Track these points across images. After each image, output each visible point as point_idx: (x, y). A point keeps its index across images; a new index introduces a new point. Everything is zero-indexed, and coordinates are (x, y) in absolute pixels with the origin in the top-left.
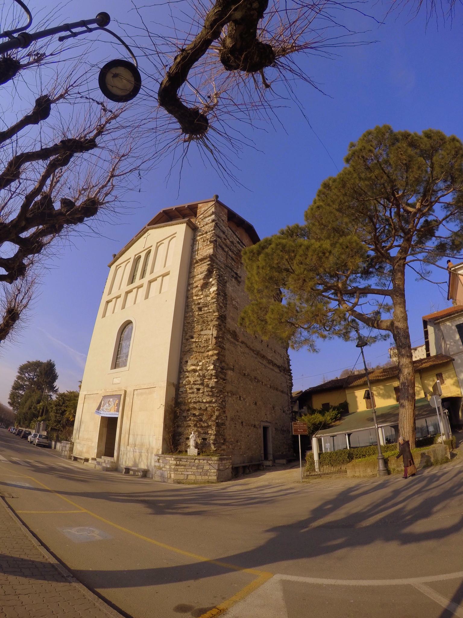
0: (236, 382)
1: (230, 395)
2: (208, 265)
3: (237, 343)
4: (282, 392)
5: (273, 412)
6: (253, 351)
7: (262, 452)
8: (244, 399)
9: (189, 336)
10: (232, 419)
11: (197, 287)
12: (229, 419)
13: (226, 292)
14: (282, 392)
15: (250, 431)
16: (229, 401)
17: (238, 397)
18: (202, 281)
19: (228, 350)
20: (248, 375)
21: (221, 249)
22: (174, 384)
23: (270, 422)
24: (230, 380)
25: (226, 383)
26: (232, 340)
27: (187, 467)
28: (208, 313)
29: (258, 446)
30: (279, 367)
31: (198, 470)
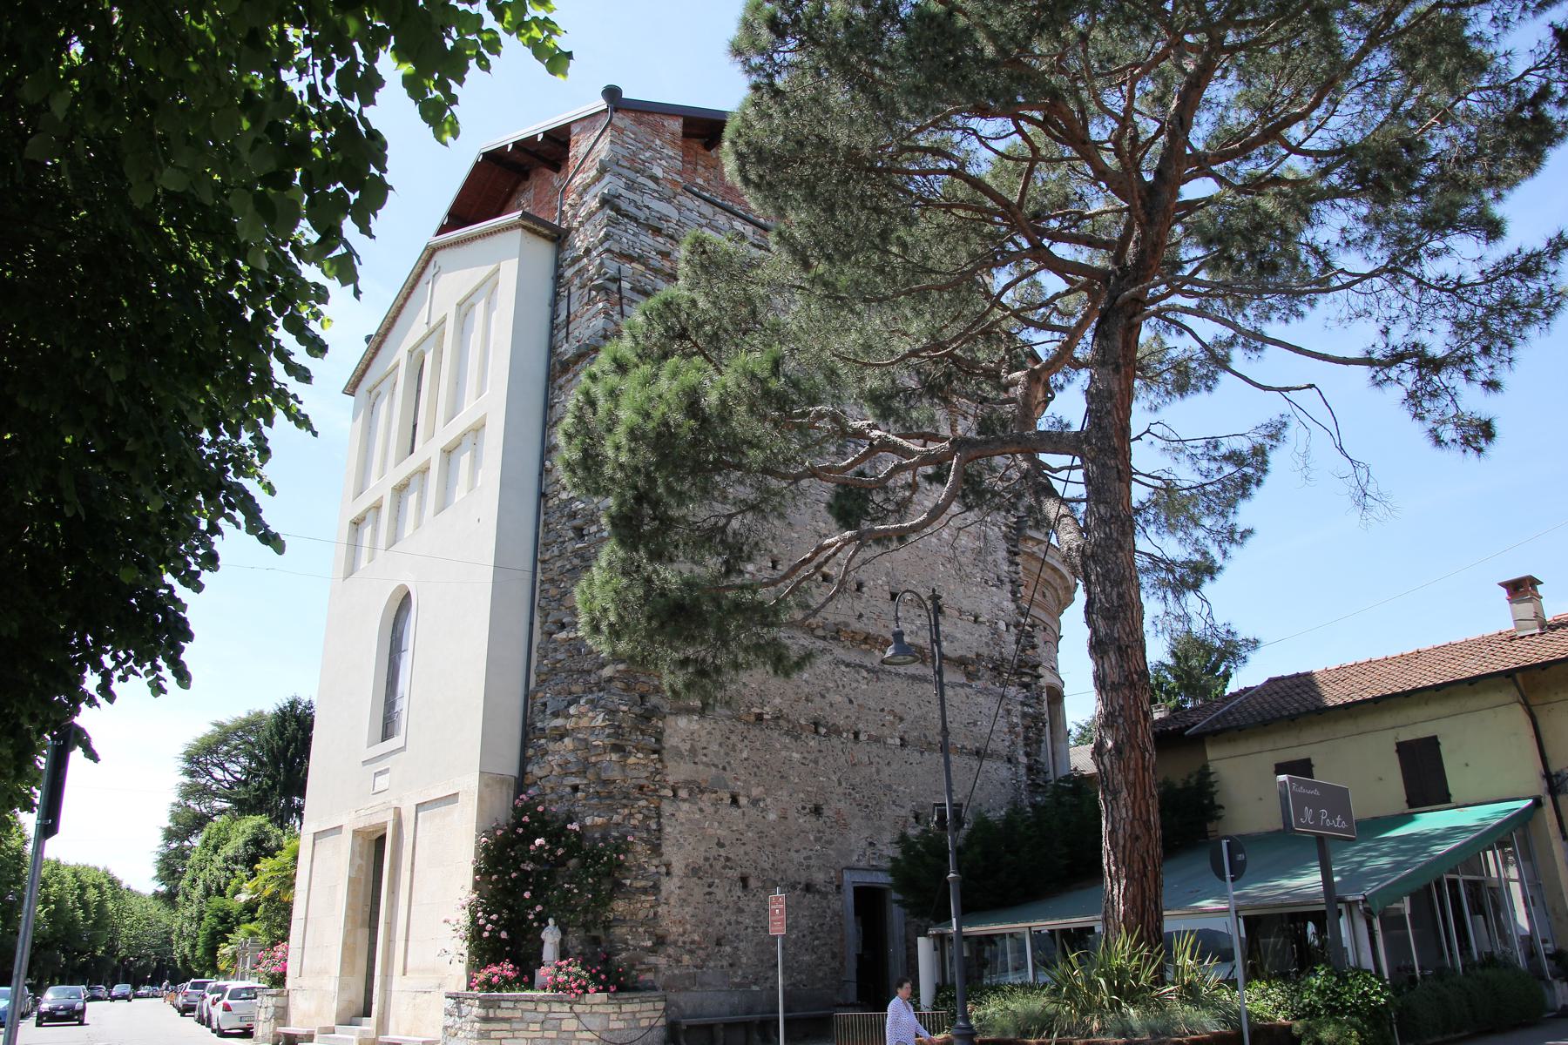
0: (716, 748)
9: (554, 623)
10: (695, 871)
12: (678, 867)
16: (681, 816)
22: (501, 780)
24: (685, 747)
27: (515, 1026)
31: (547, 1034)
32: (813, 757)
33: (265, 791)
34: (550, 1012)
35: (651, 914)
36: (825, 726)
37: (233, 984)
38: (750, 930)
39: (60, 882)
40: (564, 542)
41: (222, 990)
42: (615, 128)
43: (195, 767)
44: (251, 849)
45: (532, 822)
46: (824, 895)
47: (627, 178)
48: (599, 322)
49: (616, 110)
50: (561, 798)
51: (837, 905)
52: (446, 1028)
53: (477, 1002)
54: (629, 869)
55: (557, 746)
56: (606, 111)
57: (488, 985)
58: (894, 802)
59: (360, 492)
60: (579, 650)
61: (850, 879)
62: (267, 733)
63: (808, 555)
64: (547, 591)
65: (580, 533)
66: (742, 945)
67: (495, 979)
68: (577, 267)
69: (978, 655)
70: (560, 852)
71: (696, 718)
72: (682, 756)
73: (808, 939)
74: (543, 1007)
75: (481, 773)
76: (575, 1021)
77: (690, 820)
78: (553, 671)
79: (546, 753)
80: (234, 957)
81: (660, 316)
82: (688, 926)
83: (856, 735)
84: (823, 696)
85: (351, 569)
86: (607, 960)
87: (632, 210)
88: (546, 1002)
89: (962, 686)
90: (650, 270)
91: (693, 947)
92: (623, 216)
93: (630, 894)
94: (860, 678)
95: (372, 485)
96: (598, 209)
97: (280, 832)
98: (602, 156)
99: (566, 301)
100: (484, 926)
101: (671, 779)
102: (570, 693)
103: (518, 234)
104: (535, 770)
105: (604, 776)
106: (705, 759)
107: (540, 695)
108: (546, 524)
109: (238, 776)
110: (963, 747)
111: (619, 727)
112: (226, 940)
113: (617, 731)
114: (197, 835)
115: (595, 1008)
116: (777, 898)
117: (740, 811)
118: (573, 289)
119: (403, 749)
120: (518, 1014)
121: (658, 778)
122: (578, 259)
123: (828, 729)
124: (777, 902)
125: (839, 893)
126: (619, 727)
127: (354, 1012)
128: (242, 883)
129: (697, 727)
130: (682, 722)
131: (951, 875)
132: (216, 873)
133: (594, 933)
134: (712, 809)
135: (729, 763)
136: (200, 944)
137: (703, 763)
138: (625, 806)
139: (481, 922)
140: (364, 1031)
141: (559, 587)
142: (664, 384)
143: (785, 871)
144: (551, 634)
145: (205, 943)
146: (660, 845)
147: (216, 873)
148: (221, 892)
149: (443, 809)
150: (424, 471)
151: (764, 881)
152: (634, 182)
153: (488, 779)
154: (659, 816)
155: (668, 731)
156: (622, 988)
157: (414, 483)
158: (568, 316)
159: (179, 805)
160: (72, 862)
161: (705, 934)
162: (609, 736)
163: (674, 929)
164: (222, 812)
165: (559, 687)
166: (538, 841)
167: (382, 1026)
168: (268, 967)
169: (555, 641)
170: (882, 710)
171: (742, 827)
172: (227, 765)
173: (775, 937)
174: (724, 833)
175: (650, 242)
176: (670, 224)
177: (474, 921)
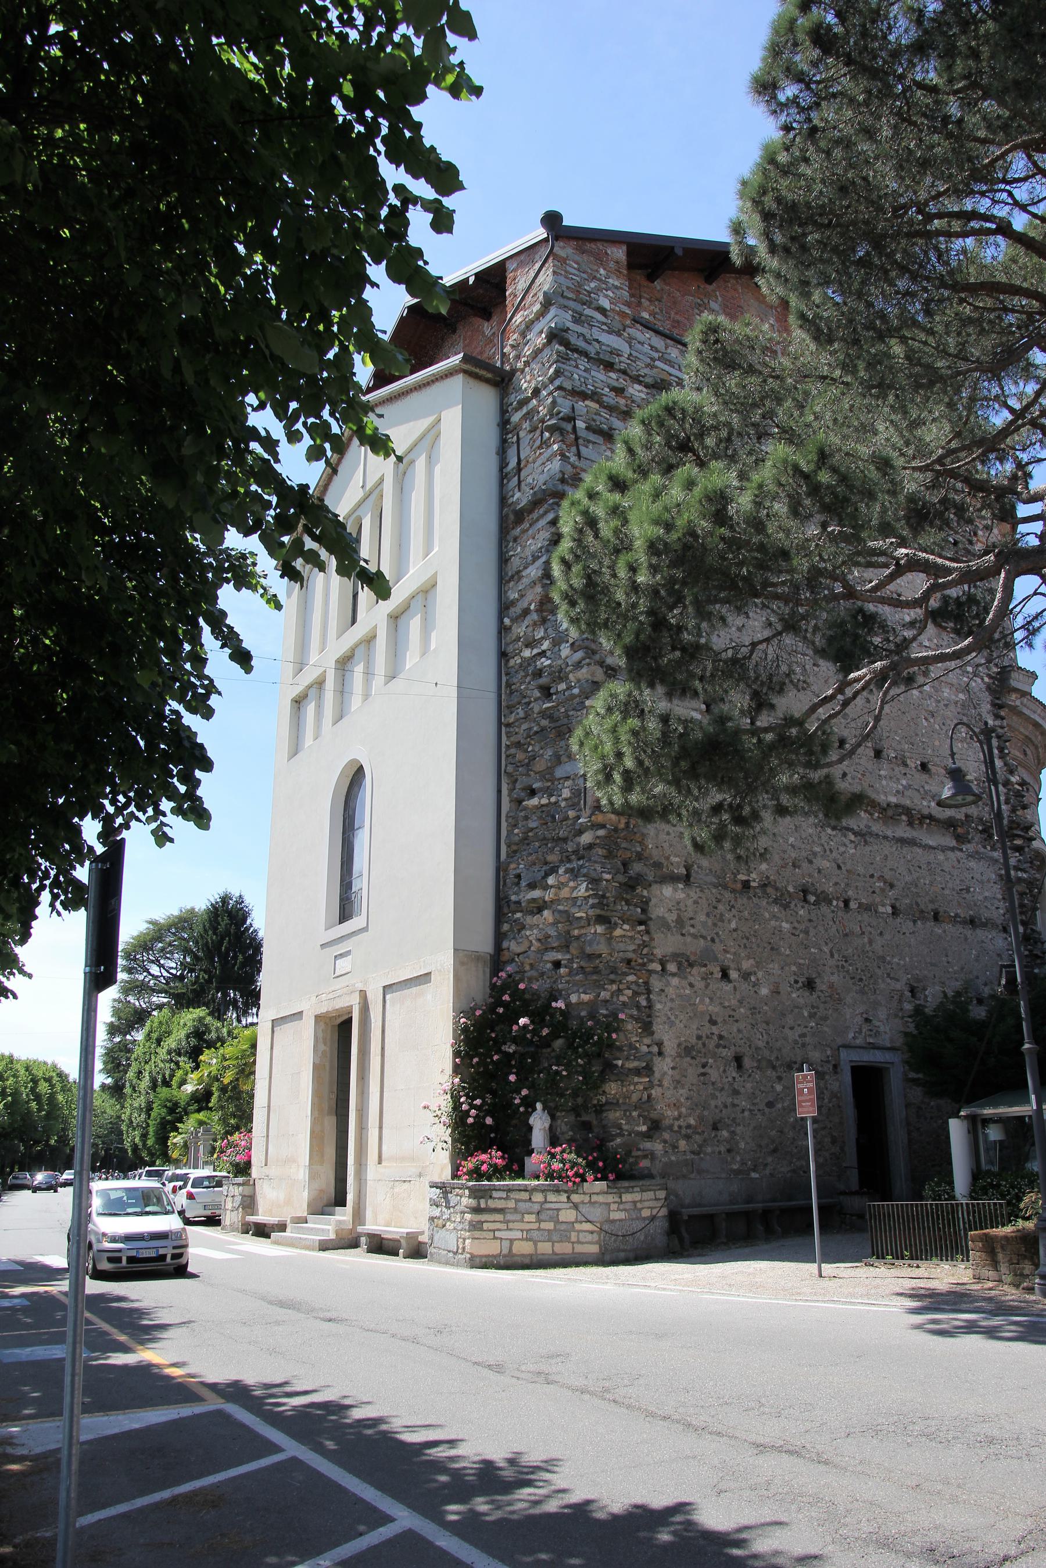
1: (672, 967)
9: (523, 789)
10: (687, 1051)
11: (526, 612)
12: (670, 1047)
16: (671, 991)
20: (764, 886)
21: (600, 440)
22: (477, 957)
24: (671, 918)
27: (509, 1217)
31: (543, 1225)
32: (803, 927)
34: (546, 1202)
35: (645, 1097)
36: (814, 894)
37: (195, 1173)
38: (746, 1113)
39: (14, 1076)
40: (529, 703)
41: (184, 1178)
42: (556, 258)
43: (133, 964)
44: (193, 1041)
45: (513, 1001)
47: (574, 311)
48: (556, 465)
49: (556, 238)
50: (542, 974)
52: (432, 1219)
53: (467, 1192)
54: (620, 1049)
55: (536, 919)
56: (546, 240)
57: (477, 1174)
58: (888, 975)
59: (300, 665)
60: (554, 817)
61: (847, 1058)
62: (201, 928)
63: (830, 692)
64: (514, 756)
65: (546, 692)
66: (739, 1130)
67: (484, 1167)
68: (525, 410)
71: (681, 886)
72: (669, 928)
74: (538, 1197)
75: (455, 950)
77: (680, 996)
78: (525, 840)
80: (186, 1145)
81: (661, 424)
82: (683, 1110)
83: (846, 903)
84: (810, 862)
85: (295, 749)
86: (601, 1146)
87: (581, 344)
88: (543, 1191)
89: (952, 849)
90: (605, 407)
91: (689, 1131)
92: (573, 350)
93: (623, 1075)
94: (847, 842)
96: (545, 346)
98: (546, 288)
100: (468, 1111)
101: (658, 952)
102: (546, 863)
103: (458, 381)
104: (513, 946)
105: (588, 950)
106: (692, 930)
107: (512, 866)
108: (509, 685)
109: (174, 971)
110: (957, 915)
111: (603, 896)
112: (176, 1129)
113: (602, 901)
114: (138, 1031)
115: (594, 1198)
116: (806, 1076)
117: (731, 985)
118: (522, 434)
119: (365, 929)
120: (511, 1204)
121: (645, 951)
122: (526, 401)
123: (817, 896)
124: (805, 1083)
125: (836, 1073)
126: (603, 896)
127: (325, 1202)
128: (186, 1074)
129: (683, 896)
130: (667, 891)
131: (1027, 1046)
132: (161, 1065)
133: (585, 1118)
134: (702, 984)
135: (717, 934)
136: (151, 1133)
137: (690, 934)
138: (613, 982)
139: (465, 1107)
140: (340, 1222)
141: (526, 751)
142: (676, 493)
143: (780, 1050)
144: (520, 802)
145: (156, 1133)
146: (651, 1023)
147: (161, 1065)
148: (167, 1084)
149: (414, 990)
150: (370, 640)
151: (759, 1061)
152: (581, 315)
153: (463, 957)
154: (649, 992)
155: (653, 901)
156: (620, 1176)
157: (359, 653)
159: (119, 1001)
160: (24, 1058)
161: (701, 1119)
162: (593, 906)
163: (669, 1113)
164: (160, 1007)
165: (534, 857)
166: (522, 1021)
167: (359, 1216)
168: (233, 1156)
169: (525, 808)
170: (872, 876)
171: (734, 1002)
172: (162, 962)
174: (716, 1010)
175: (604, 378)
176: (622, 359)
177: (456, 1106)
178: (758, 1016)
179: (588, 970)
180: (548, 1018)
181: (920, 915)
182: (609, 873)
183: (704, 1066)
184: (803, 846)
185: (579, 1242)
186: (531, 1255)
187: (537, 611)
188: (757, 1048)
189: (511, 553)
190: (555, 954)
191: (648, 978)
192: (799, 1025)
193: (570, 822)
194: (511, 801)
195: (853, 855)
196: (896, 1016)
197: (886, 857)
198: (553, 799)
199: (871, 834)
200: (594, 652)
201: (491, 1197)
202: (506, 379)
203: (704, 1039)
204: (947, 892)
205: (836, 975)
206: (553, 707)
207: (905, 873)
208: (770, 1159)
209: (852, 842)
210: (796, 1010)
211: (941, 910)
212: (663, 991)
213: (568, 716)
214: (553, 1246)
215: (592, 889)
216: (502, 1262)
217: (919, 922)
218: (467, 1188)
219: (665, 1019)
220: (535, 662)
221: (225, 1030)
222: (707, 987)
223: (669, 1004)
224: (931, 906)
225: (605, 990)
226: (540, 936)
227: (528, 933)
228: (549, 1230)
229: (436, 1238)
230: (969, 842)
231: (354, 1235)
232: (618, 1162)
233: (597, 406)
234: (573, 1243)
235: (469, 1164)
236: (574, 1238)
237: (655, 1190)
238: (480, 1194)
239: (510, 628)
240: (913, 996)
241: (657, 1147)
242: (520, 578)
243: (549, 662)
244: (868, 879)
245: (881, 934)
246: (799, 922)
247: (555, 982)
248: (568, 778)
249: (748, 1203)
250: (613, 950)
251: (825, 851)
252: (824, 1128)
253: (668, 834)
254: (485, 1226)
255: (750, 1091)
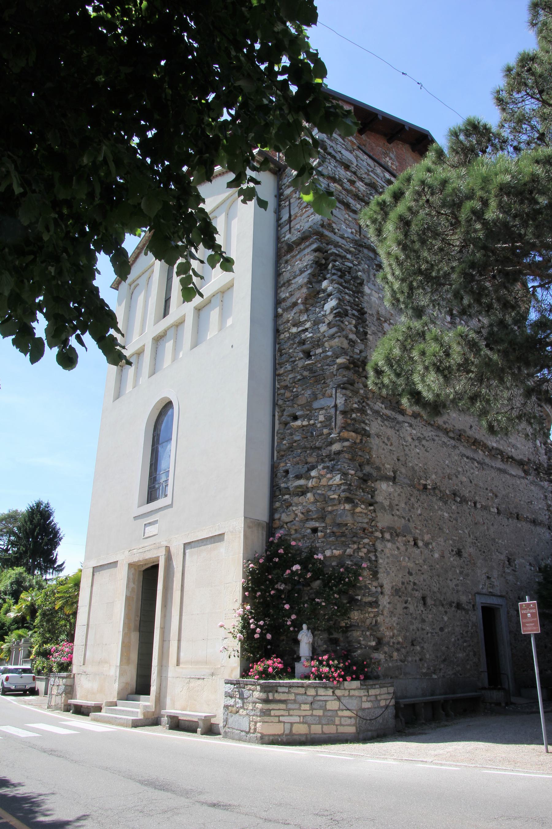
1: (387, 536)
2: (315, 250)
3: (400, 418)
4: (534, 522)
5: (507, 571)
6: (446, 432)
7: (483, 667)
8: (427, 544)
9: (289, 416)
10: (397, 592)
11: (295, 304)
13: (365, 305)
14: (534, 522)
15: (446, 618)
16: (387, 551)
17: (411, 539)
18: (304, 290)
19: (378, 436)
20: (434, 489)
21: (342, 207)
22: (258, 524)
23: (501, 596)
24: (386, 503)
25: (375, 511)
26: (388, 412)
27: (290, 706)
28: (323, 358)
29: (471, 653)
30: (521, 463)
31: (316, 712)
33: (21, 554)
34: (317, 695)
36: (459, 497)
38: (429, 635)
40: (294, 361)
46: (467, 611)
50: (304, 537)
51: (474, 619)
52: (226, 707)
53: (258, 688)
57: (264, 674)
58: (497, 550)
60: (312, 433)
61: (481, 601)
65: (308, 355)
69: (529, 460)
70: (309, 575)
73: (460, 642)
74: (311, 692)
75: (245, 518)
76: (337, 703)
77: (392, 555)
78: (291, 448)
79: (291, 505)
80: (9, 651)
83: (475, 503)
84: (457, 477)
85: (118, 394)
88: (315, 687)
89: (523, 478)
91: (399, 646)
94: (474, 467)
95: (134, 341)
97: (31, 577)
99: (287, 208)
100: (255, 629)
101: (380, 525)
102: (307, 463)
105: (339, 520)
106: (398, 513)
107: (282, 464)
110: (527, 517)
111: (350, 485)
115: (352, 693)
118: (292, 201)
119: (171, 506)
120: (292, 697)
121: (373, 524)
123: (461, 498)
126: (350, 485)
127: (129, 691)
129: (392, 490)
133: (335, 635)
135: (411, 516)
137: (397, 515)
138: (354, 543)
139: (252, 626)
140: (146, 706)
143: (445, 594)
144: (286, 424)
150: (179, 324)
151: (435, 600)
154: (376, 550)
156: (367, 678)
157: (170, 333)
158: (290, 216)
162: (344, 491)
163: (387, 633)
167: (160, 701)
169: (291, 428)
171: (421, 561)
173: (529, 636)
177: (246, 625)
178: (434, 571)
179: (337, 534)
180: (311, 566)
181: (510, 515)
182: (353, 470)
183: (406, 602)
184: (453, 467)
185: (341, 725)
186: (306, 734)
187: (303, 303)
188: (434, 592)
189: (284, 270)
190: (314, 523)
191: (375, 542)
192: (455, 578)
193: (324, 437)
194: (280, 423)
195: (477, 475)
196: (502, 576)
197: (493, 479)
198: (312, 422)
199: (485, 463)
200: (343, 330)
201: (277, 691)
202: (282, 170)
203: (406, 584)
204: (522, 503)
205: (472, 548)
206: (312, 363)
207: (502, 489)
208: (442, 666)
209: (476, 467)
210: (453, 569)
211: (520, 513)
212: (382, 551)
213: (323, 370)
214: (322, 728)
215: (344, 480)
216: (285, 740)
217: (510, 519)
218: (259, 685)
219: (384, 570)
220: (299, 336)
221: (34, 581)
222: (406, 550)
223: (386, 560)
224: (515, 511)
225: (349, 548)
226: (304, 511)
227: (294, 508)
228: (319, 716)
229: (230, 720)
230: (530, 475)
231: (156, 716)
232: (365, 666)
233: (340, 188)
234: (337, 725)
235: (259, 667)
236: (337, 722)
237: (387, 687)
238: (268, 689)
239: (282, 315)
240: (509, 564)
241: (382, 656)
242: (290, 285)
243: (311, 335)
244: (485, 491)
245: (493, 524)
246: (452, 513)
247: (313, 542)
248: (322, 409)
249: (432, 695)
250: (355, 521)
251: (464, 471)
252: (470, 646)
253: (384, 449)
254: (273, 713)
255: (431, 620)
